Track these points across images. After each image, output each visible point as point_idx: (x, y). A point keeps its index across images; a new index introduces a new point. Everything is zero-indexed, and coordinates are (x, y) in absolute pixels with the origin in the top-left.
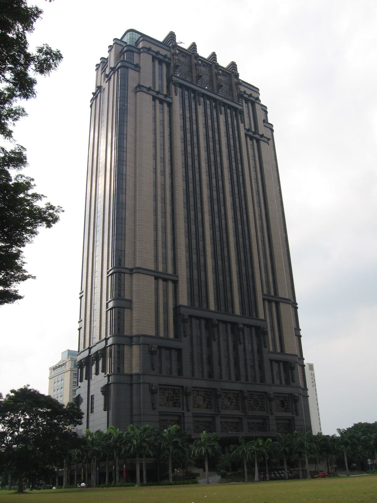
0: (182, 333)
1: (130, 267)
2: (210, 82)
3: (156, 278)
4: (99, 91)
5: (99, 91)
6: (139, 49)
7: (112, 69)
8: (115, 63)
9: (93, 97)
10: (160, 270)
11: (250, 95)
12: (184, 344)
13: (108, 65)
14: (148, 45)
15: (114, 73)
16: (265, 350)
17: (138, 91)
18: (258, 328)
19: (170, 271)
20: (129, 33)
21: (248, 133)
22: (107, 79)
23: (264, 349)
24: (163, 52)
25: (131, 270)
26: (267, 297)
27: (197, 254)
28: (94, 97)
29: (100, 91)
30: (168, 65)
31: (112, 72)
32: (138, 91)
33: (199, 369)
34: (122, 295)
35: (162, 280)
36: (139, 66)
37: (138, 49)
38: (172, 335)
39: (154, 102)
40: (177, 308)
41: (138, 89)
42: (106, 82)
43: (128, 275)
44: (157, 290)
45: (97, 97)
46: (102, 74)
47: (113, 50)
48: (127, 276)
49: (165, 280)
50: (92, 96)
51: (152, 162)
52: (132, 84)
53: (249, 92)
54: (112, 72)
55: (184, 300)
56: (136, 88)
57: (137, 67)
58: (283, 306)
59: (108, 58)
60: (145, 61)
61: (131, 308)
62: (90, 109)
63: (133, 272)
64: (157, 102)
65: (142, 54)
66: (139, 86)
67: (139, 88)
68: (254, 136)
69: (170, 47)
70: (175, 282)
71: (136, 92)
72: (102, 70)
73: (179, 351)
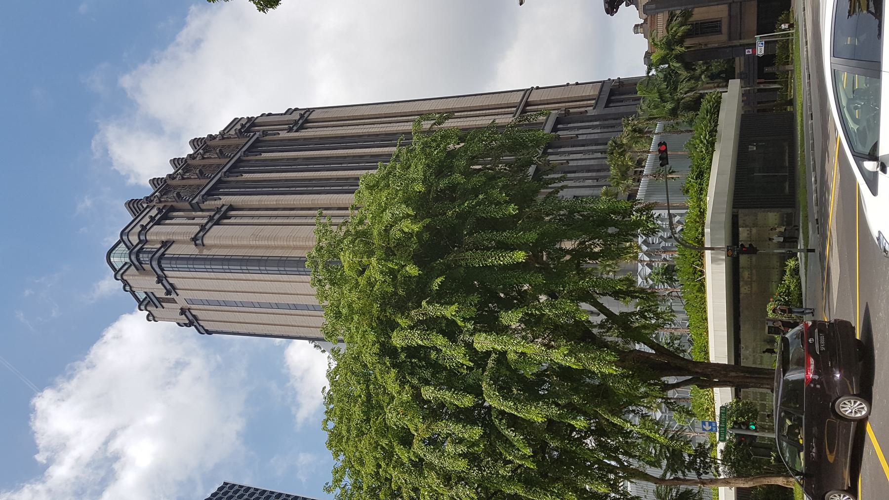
6: (140, 241)
15: (166, 277)
18: (558, 121)
20: (112, 259)
29: (189, 309)
53: (238, 127)
56: (196, 245)
57: (166, 244)
60: (158, 233)
66: (194, 239)
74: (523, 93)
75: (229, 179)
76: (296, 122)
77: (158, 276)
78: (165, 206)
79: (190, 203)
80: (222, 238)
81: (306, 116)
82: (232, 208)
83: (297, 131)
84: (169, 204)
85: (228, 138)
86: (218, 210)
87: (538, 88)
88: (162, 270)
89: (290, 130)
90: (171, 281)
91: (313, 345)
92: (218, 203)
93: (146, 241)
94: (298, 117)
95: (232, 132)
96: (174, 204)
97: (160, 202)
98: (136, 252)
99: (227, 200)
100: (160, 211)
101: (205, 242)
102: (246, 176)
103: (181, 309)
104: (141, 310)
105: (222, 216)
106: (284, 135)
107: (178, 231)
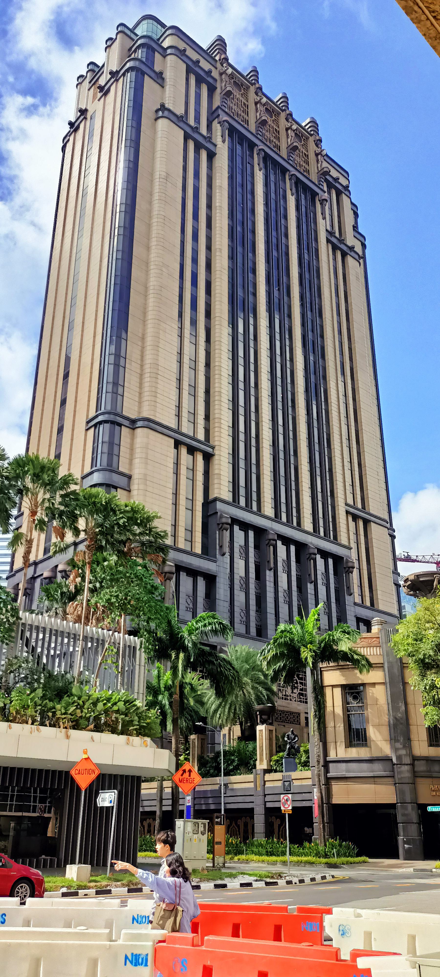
0: (218, 547)
1: (133, 417)
2: (398, 745)
3: (177, 444)
4: (82, 117)
5: (82, 117)
6: (165, 50)
7: (114, 74)
8: (121, 59)
9: (69, 131)
10: (184, 430)
11: (336, 180)
12: (219, 567)
13: (103, 72)
14: (182, 45)
15: (117, 80)
16: (348, 600)
17: (168, 54)
18: (338, 560)
19: (201, 436)
20: (145, 22)
21: (330, 238)
22: (99, 95)
23: (347, 597)
24: (205, 65)
25: (133, 422)
26: (352, 510)
27: (245, 390)
28: (72, 130)
29: (85, 118)
30: (212, 90)
31: (113, 80)
32: (168, 54)
33: (242, 618)
34: (115, 465)
35: (185, 574)
36: (163, 76)
37: (162, 48)
38: (198, 549)
39: (176, 450)
40: (208, 504)
41: (160, 113)
42: (99, 100)
43: (128, 429)
44: (177, 464)
45: (78, 128)
46: (89, 90)
47: (116, 46)
48: (125, 431)
49: (192, 450)
50: (67, 129)
51: (175, 366)
52: (149, 105)
53: (334, 174)
54: (113, 80)
55: (222, 489)
56: (157, 111)
57: (159, 78)
58: (374, 528)
59: (103, 65)
60: (173, 69)
61: (128, 489)
62: (62, 154)
63: (137, 426)
64: (184, 451)
65: (169, 58)
66: (163, 107)
67: (163, 110)
68: (339, 245)
69: (216, 61)
70: (208, 457)
71: (156, 119)
72: (90, 82)
73: (211, 580)
74: (387, 518)
75: (255, 156)
76: (342, 241)
77: (117, 72)
78: (216, 80)
79: (218, 107)
80: (165, 142)
81: (352, 254)
82: (211, 156)
83: (328, 241)
84: (218, 85)
85: (318, 161)
86: (209, 139)
87: (393, 537)
88: (124, 75)
89: (331, 233)
90: (113, 89)
91: (395, 534)
92: (218, 139)
93: (164, 57)
94: (350, 244)
95: (325, 164)
96: (218, 91)
97: (221, 74)
98: (152, 46)
99: (223, 150)
100: (209, 73)
101: (160, 121)
102: (291, 201)
103: (86, 110)
104: (88, 65)
105: (197, 143)
106: (323, 226)
107: (174, 88)
